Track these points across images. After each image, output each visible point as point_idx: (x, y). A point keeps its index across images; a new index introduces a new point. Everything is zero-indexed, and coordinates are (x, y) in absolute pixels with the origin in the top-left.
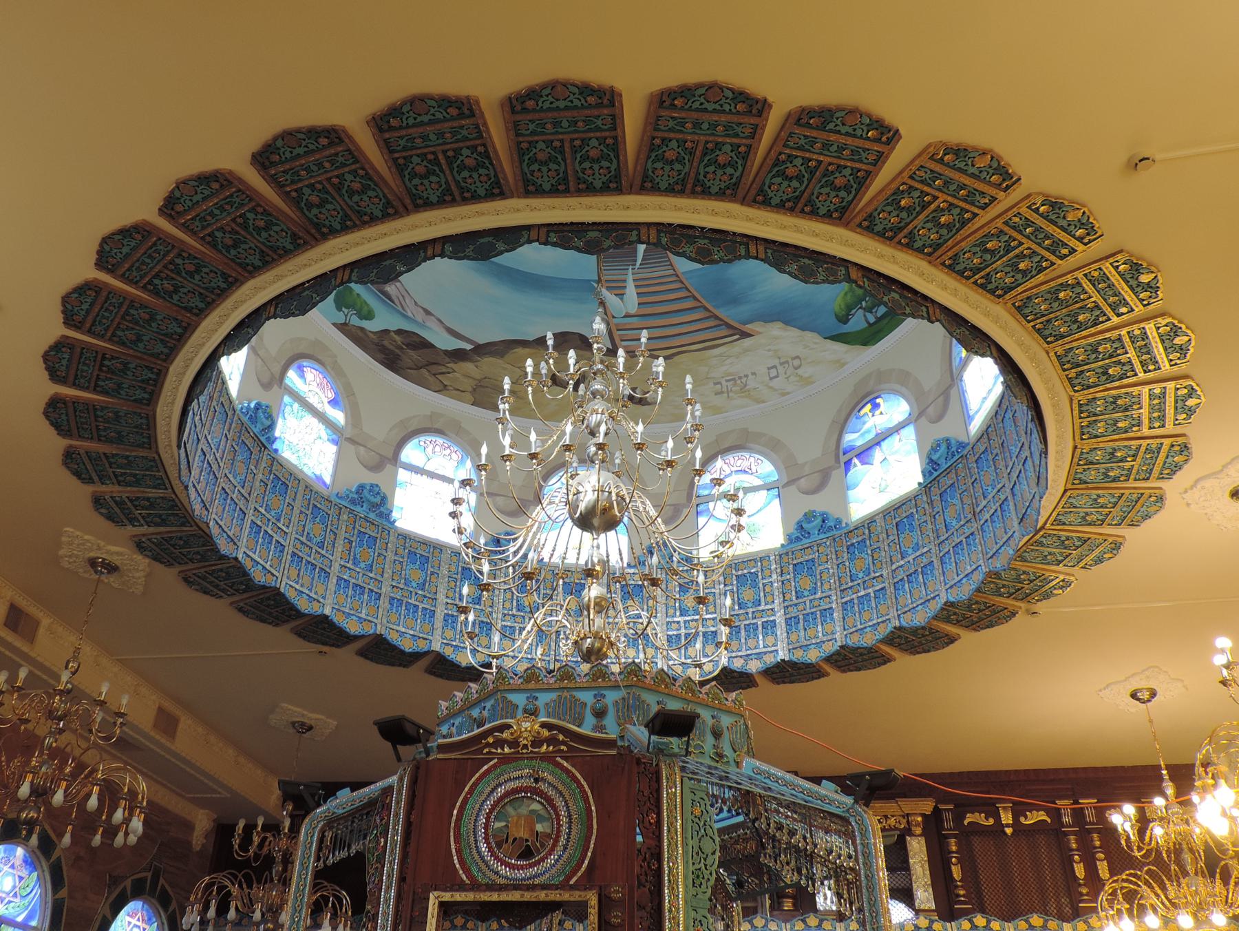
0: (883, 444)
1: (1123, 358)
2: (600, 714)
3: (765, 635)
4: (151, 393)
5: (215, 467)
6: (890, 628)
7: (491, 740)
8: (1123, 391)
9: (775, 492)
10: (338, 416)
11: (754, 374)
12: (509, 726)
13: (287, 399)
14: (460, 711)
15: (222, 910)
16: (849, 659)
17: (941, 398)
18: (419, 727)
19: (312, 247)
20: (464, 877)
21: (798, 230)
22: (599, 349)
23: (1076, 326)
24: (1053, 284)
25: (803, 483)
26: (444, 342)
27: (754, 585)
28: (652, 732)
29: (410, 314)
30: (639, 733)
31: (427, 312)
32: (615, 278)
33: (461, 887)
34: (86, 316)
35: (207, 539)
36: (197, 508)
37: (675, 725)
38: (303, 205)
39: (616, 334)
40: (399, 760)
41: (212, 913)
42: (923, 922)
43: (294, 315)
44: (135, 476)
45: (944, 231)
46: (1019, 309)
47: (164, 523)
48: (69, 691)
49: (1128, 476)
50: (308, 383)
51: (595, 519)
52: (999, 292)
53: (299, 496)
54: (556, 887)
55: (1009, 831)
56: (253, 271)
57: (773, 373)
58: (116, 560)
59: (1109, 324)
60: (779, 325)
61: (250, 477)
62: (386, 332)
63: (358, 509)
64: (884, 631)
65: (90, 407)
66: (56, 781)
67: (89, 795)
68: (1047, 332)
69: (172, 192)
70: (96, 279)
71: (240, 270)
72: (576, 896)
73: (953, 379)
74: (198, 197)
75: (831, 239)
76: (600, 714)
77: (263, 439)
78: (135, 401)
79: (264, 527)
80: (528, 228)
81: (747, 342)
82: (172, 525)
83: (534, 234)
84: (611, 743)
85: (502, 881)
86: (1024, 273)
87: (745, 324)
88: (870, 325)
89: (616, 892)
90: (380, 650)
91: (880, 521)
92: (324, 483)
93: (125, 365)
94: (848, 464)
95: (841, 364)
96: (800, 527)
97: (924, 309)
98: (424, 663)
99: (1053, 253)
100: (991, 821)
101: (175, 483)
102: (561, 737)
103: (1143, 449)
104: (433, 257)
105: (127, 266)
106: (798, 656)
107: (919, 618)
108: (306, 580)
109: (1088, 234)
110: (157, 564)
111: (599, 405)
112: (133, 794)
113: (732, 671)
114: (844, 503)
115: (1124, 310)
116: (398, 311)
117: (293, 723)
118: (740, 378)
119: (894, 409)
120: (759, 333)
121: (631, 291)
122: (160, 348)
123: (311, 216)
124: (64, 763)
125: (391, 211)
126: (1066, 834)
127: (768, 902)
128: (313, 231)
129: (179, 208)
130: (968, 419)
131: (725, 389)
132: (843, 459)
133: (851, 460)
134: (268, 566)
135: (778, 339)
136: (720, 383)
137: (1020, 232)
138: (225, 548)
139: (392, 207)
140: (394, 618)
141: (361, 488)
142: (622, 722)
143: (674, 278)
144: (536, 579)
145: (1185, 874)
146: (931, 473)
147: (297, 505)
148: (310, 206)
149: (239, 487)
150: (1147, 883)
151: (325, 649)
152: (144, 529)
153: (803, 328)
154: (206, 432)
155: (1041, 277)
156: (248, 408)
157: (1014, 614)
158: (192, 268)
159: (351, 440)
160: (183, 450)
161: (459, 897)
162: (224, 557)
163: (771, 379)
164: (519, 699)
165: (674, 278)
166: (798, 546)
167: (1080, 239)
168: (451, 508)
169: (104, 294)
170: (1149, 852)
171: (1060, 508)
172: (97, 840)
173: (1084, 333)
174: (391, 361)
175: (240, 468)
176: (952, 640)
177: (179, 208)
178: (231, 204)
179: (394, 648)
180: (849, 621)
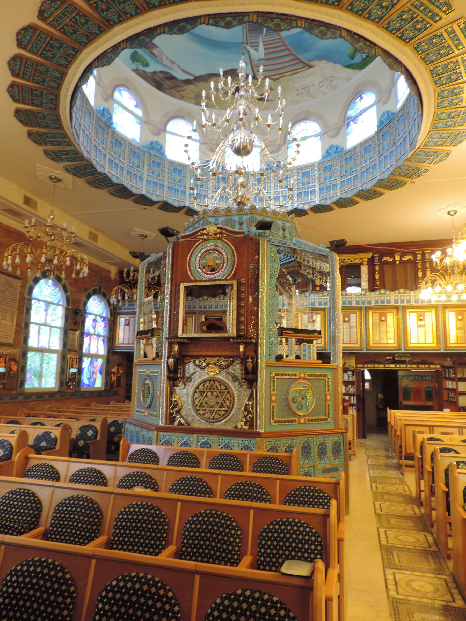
1: (458, 71)
2: (241, 224)
3: (311, 195)
4: (56, 105)
5: (90, 136)
6: (357, 190)
7: (199, 234)
8: (457, 86)
10: (139, 112)
11: (313, 85)
12: (205, 229)
13: (116, 105)
14: (192, 225)
15: (123, 297)
16: (343, 203)
17: (388, 94)
18: (174, 230)
19: (108, 32)
21: (319, 12)
22: (242, 76)
23: (439, 56)
24: (431, 35)
25: (330, 133)
26: (181, 76)
27: (308, 176)
28: (257, 229)
29: (165, 63)
30: (253, 229)
31: (173, 62)
33: (191, 281)
34: (19, 71)
35: (91, 166)
36: (85, 154)
37: (265, 226)
38: (99, 10)
40: (168, 242)
41: (120, 298)
42: (363, 292)
43: (105, 65)
44: (58, 141)
45: (384, 10)
46: (416, 48)
47: (74, 160)
48: (52, 226)
49: (455, 124)
50: (124, 97)
51: (242, 151)
52: (407, 40)
53: (127, 147)
54: (223, 280)
55: (397, 263)
56: (85, 45)
57: (321, 84)
58: (59, 177)
59: (453, 54)
60: (324, 61)
61: (105, 140)
62: (155, 73)
63: (151, 151)
64: (355, 191)
65: (33, 113)
66: (54, 256)
67: (66, 261)
68: (426, 60)
69: (41, 7)
70: (19, 53)
71: (79, 45)
72: (229, 282)
73: (394, 83)
74: (52, 9)
75: (334, 16)
76: (241, 224)
77: (108, 123)
78: (50, 109)
79: (114, 161)
80: (200, 17)
81: (311, 70)
82: (78, 161)
83: (203, 20)
84: (242, 233)
85: (204, 279)
86: (419, 30)
87: (310, 61)
89: (243, 281)
90: (166, 207)
91: (358, 148)
92: (136, 142)
93: (42, 92)
94: (348, 124)
95: (349, 79)
96: (327, 152)
97: (374, 50)
98: (184, 211)
99: (432, 19)
100: (392, 260)
101: (74, 143)
102: (224, 232)
103: (462, 112)
104: (160, 34)
105: (30, 46)
106: (323, 203)
107: (369, 186)
108: (134, 181)
109: (448, 9)
110: (75, 177)
111: (243, 102)
112: (83, 260)
113: (299, 210)
114: (345, 140)
115: (461, 47)
116: (159, 62)
117: (140, 235)
119: (369, 98)
120: (316, 66)
121: (261, 47)
122: (54, 84)
123: (104, 15)
124: (55, 250)
125: (139, 11)
126: (418, 263)
127: (311, 288)
128: (107, 23)
129: (46, 15)
130: (397, 102)
132: (347, 122)
134: (118, 176)
135: (324, 68)
137: (418, 9)
138: (99, 169)
139: (139, 9)
140: (170, 194)
141: (152, 143)
142: (249, 226)
143: (280, 40)
144: (221, 175)
145: (454, 273)
146: (380, 127)
147: (127, 151)
148: (103, 11)
149: (101, 145)
150: (439, 276)
151: (147, 207)
152: (67, 163)
153: (335, 62)
154: (83, 121)
155: (426, 32)
156: (100, 110)
157: (405, 184)
158: (58, 45)
159: (146, 123)
160: (74, 129)
161: (190, 284)
162: (100, 173)
163: (320, 87)
164: (212, 220)
166: (326, 159)
167: (445, 12)
168: (185, 148)
169: (24, 60)
170: (443, 267)
171: (426, 140)
172: (74, 275)
173: (442, 59)
174: (159, 86)
175: (101, 136)
176: (381, 194)
177: (46, 15)
178: (68, 11)
179: (171, 206)
180: (343, 188)
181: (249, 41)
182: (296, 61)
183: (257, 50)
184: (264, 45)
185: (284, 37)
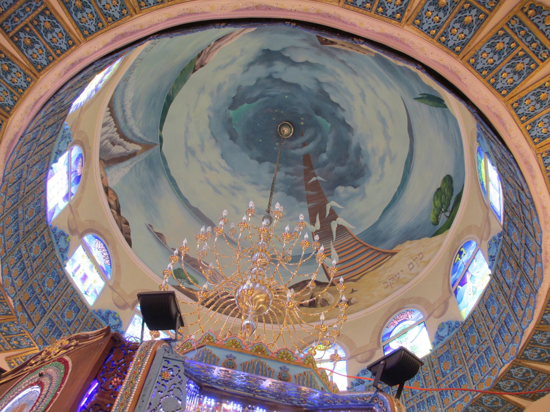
0: (469, 270)
9: (423, 324)
11: (402, 271)
57: (411, 266)
60: (408, 242)
81: (395, 257)
88: (448, 217)
114: (459, 311)
118: (395, 276)
131: (389, 284)
132: (453, 290)
133: (456, 288)
141: (109, 313)
143: (353, 240)
153: (419, 238)
159: (111, 287)
163: (411, 270)
165: (353, 240)
182: (376, 254)
184: (336, 250)
185: (357, 236)
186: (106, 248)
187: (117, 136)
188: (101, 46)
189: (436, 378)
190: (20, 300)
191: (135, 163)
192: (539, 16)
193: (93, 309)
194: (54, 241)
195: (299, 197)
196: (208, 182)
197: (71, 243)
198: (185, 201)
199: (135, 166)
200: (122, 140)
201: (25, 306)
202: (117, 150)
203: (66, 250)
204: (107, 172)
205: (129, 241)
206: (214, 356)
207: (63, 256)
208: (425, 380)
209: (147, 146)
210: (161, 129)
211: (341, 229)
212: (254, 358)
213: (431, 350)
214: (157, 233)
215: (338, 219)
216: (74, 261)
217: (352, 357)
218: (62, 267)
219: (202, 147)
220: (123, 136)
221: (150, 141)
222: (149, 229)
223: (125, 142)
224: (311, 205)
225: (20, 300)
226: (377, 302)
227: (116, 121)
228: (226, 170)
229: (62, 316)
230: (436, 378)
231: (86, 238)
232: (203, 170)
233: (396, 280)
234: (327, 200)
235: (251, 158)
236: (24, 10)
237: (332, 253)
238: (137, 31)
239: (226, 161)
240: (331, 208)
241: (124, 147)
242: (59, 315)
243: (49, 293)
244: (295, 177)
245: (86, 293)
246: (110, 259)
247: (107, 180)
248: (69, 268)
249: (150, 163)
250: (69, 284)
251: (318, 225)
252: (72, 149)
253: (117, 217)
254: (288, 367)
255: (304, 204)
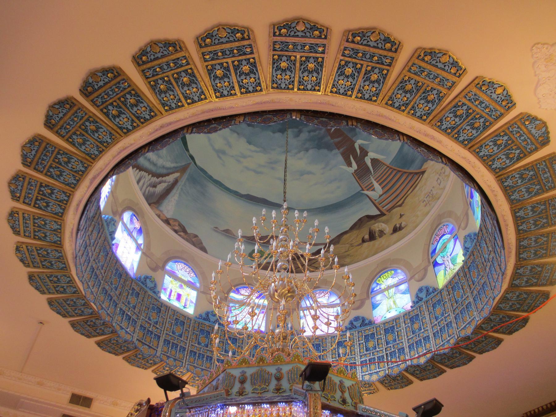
11: (433, 187)
20: (95, 307)
27: (393, 332)
32: (368, 184)
39: (380, 206)
57: (439, 181)
81: (425, 175)
96: (417, 297)
120: (427, 168)
121: (376, 185)
136: (424, 201)
159: (203, 292)
163: (439, 185)
181: (363, 187)
183: (374, 190)
185: (390, 164)
186: (187, 265)
187: (155, 179)
188: (86, 189)
189: (469, 286)
190: (137, 339)
191: (180, 188)
192: (364, 38)
193: (195, 315)
194: (144, 286)
195: (329, 148)
196: (247, 168)
197: (156, 280)
198: (236, 194)
199: (182, 189)
200: (161, 178)
201: (143, 341)
202: (160, 188)
203: (155, 286)
204: (161, 208)
205: (204, 249)
206: (232, 375)
207: (154, 292)
208: (463, 289)
209: (183, 170)
210: (187, 150)
211: (374, 161)
212: (258, 368)
213: (463, 261)
214: (224, 231)
215: (369, 154)
216: (165, 289)
217: (411, 278)
218: (158, 299)
219: (229, 145)
220: (158, 176)
221: (183, 164)
222: (216, 231)
223: (164, 179)
224: (341, 150)
225: (137, 339)
226: (421, 221)
227: (146, 170)
228: (257, 152)
229: (173, 333)
230: (469, 286)
231: (168, 267)
232: (239, 161)
233: (432, 197)
234: (353, 141)
235: (274, 132)
236: (30, 189)
237: (375, 186)
238: (98, 175)
239: (254, 145)
240: (359, 146)
241: (165, 182)
242: (171, 334)
243: (156, 323)
244: (317, 132)
245: (185, 307)
246: (194, 272)
247: (164, 215)
248: (164, 297)
249: (193, 180)
250: (168, 308)
251: (355, 166)
252: (123, 219)
253: (185, 237)
254: (281, 367)
255: (336, 151)
